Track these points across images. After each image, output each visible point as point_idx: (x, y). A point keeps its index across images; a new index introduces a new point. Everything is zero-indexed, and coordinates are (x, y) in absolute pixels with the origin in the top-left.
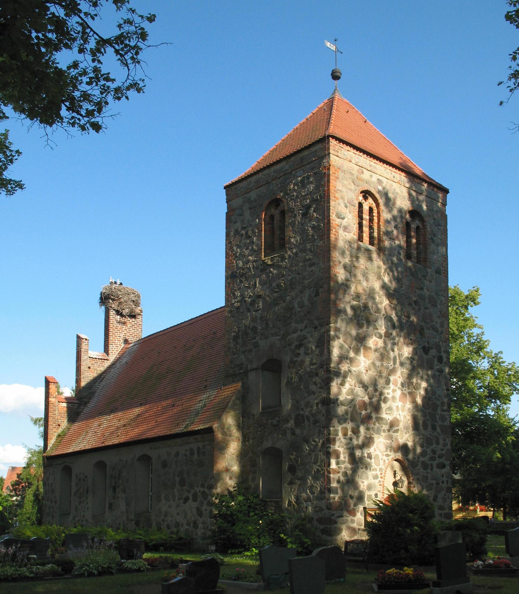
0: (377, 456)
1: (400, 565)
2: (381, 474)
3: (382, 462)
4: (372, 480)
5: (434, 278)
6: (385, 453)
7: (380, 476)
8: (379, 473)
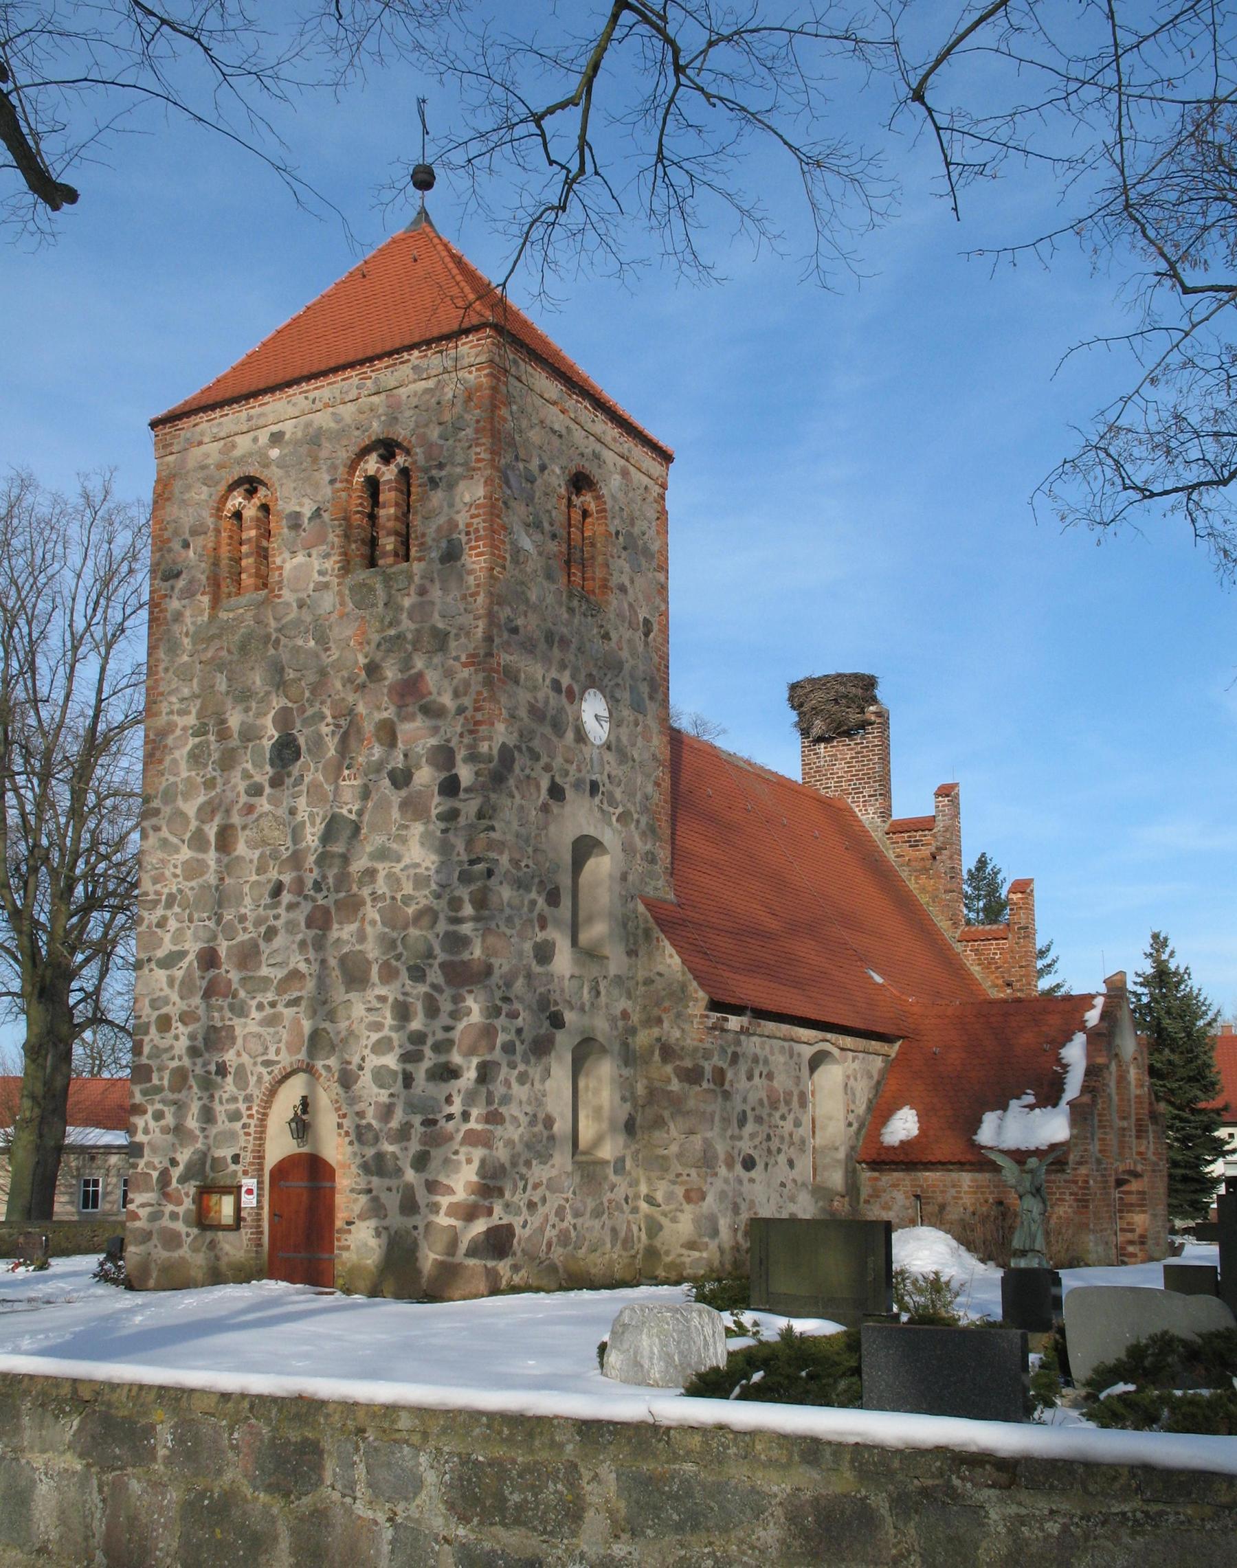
0: (241, 1069)
1: (1192, 1402)
2: (249, 1108)
3: (253, 1080)
4: (227, 1123)
5: (447, 700)
6: (260, 1059)
7: (245, 1113)
8: (242, 1106)
